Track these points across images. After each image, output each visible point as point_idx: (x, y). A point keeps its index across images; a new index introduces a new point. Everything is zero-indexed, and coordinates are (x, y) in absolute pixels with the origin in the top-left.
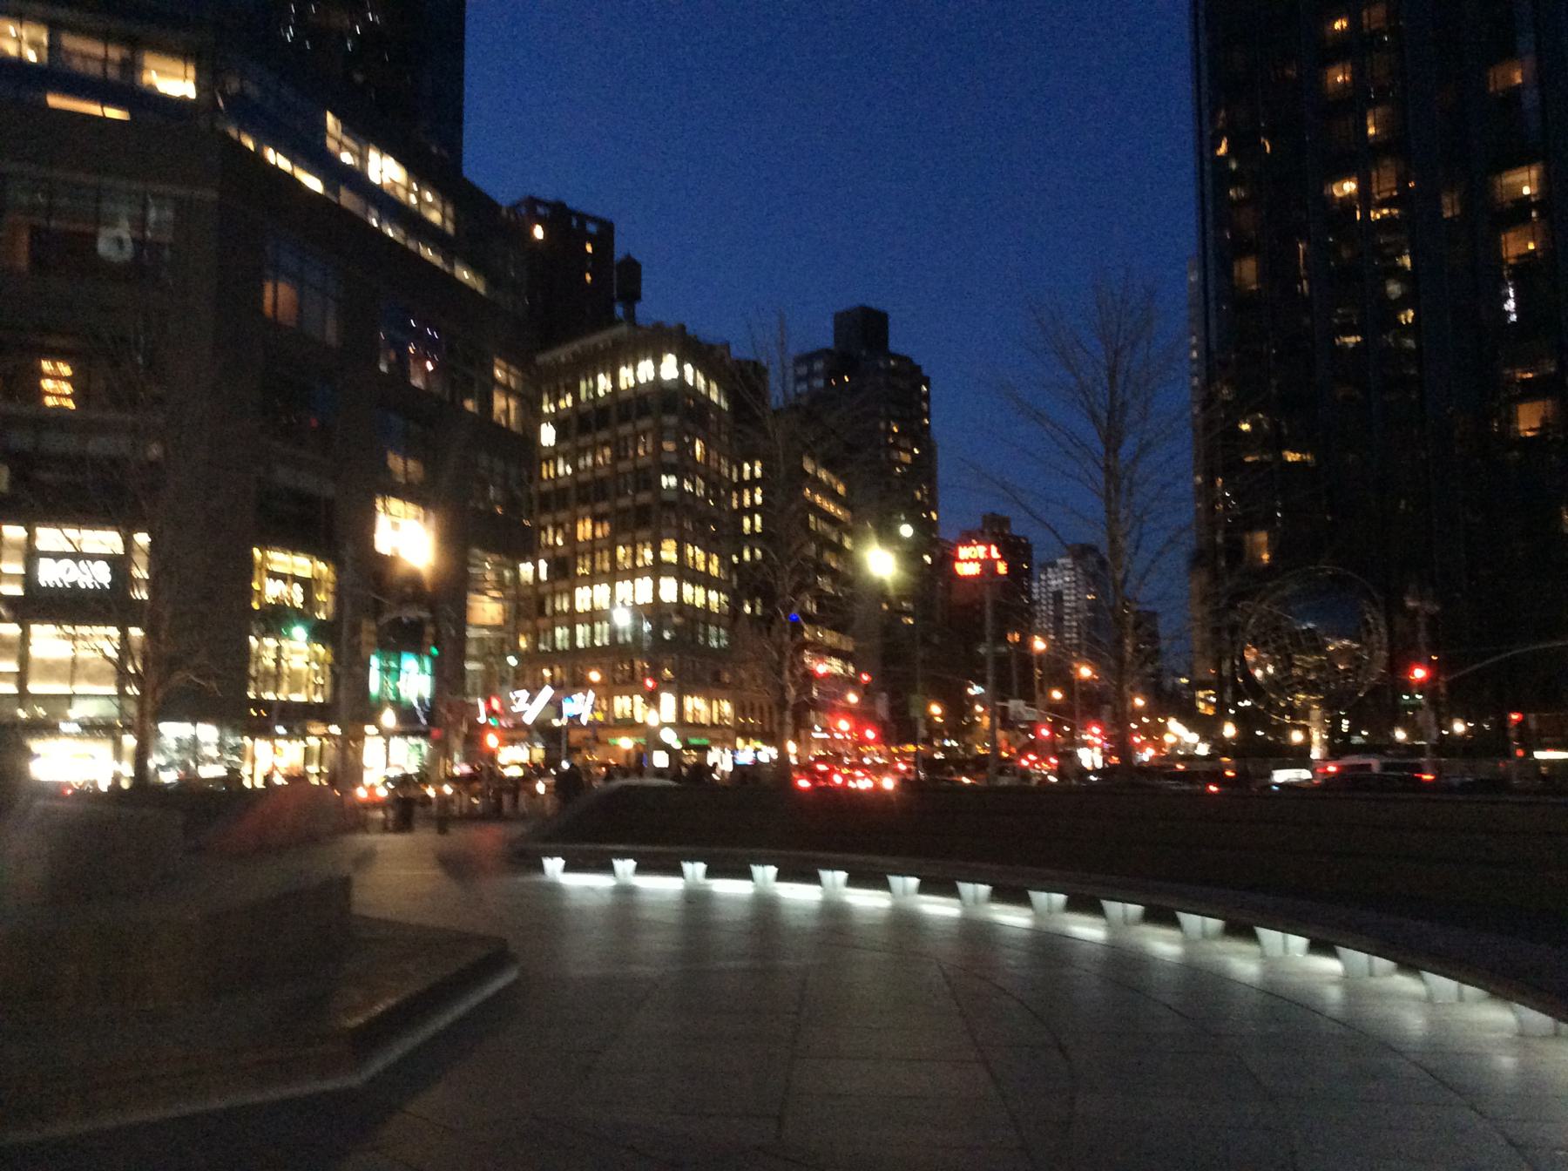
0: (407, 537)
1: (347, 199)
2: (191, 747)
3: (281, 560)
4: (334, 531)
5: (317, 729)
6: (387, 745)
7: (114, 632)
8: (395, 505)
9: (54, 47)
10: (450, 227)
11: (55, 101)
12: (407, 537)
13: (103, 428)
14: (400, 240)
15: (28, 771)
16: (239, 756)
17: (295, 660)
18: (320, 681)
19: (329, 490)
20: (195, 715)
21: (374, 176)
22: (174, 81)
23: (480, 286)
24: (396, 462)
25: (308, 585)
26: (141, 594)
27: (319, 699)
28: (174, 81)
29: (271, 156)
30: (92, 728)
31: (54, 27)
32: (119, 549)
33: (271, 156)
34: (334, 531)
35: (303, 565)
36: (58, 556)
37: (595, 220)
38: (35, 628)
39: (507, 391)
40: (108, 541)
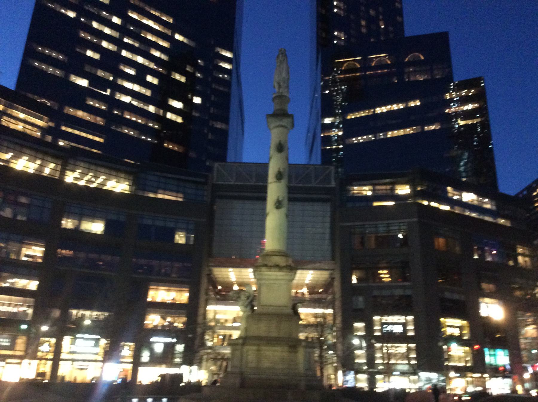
0: (492, 310)
1: (457, 210)
2: (427, 379)
3: (449, 321)
4: (466, 310)
5: (470, 374)
6: (101, 375)
7: (406, 345)
8: (487, 300)
9: (374, 190)
10: (494, 208)
11: (376, 204)
12: (492, 310)
13: (397, 287)
14: (477, 217)
16: (445, 382)
17: (458, 352)
18: (468, 359)
19: (462, 298)
20: (430, 370)
21: (464, 200)
22: (404, 190)
23: (508, 224)
24: (484, 286)
25: (461, 328)
27: (469, 365)
28: (404, 190)
29: (378, 110)
30: (403, 373)
31: (374, 185)
33: (378, 110)
34: (466, 310)
35: (458, 322)
37: (524, 190)
39: (523, 255)
40: (402, 319)
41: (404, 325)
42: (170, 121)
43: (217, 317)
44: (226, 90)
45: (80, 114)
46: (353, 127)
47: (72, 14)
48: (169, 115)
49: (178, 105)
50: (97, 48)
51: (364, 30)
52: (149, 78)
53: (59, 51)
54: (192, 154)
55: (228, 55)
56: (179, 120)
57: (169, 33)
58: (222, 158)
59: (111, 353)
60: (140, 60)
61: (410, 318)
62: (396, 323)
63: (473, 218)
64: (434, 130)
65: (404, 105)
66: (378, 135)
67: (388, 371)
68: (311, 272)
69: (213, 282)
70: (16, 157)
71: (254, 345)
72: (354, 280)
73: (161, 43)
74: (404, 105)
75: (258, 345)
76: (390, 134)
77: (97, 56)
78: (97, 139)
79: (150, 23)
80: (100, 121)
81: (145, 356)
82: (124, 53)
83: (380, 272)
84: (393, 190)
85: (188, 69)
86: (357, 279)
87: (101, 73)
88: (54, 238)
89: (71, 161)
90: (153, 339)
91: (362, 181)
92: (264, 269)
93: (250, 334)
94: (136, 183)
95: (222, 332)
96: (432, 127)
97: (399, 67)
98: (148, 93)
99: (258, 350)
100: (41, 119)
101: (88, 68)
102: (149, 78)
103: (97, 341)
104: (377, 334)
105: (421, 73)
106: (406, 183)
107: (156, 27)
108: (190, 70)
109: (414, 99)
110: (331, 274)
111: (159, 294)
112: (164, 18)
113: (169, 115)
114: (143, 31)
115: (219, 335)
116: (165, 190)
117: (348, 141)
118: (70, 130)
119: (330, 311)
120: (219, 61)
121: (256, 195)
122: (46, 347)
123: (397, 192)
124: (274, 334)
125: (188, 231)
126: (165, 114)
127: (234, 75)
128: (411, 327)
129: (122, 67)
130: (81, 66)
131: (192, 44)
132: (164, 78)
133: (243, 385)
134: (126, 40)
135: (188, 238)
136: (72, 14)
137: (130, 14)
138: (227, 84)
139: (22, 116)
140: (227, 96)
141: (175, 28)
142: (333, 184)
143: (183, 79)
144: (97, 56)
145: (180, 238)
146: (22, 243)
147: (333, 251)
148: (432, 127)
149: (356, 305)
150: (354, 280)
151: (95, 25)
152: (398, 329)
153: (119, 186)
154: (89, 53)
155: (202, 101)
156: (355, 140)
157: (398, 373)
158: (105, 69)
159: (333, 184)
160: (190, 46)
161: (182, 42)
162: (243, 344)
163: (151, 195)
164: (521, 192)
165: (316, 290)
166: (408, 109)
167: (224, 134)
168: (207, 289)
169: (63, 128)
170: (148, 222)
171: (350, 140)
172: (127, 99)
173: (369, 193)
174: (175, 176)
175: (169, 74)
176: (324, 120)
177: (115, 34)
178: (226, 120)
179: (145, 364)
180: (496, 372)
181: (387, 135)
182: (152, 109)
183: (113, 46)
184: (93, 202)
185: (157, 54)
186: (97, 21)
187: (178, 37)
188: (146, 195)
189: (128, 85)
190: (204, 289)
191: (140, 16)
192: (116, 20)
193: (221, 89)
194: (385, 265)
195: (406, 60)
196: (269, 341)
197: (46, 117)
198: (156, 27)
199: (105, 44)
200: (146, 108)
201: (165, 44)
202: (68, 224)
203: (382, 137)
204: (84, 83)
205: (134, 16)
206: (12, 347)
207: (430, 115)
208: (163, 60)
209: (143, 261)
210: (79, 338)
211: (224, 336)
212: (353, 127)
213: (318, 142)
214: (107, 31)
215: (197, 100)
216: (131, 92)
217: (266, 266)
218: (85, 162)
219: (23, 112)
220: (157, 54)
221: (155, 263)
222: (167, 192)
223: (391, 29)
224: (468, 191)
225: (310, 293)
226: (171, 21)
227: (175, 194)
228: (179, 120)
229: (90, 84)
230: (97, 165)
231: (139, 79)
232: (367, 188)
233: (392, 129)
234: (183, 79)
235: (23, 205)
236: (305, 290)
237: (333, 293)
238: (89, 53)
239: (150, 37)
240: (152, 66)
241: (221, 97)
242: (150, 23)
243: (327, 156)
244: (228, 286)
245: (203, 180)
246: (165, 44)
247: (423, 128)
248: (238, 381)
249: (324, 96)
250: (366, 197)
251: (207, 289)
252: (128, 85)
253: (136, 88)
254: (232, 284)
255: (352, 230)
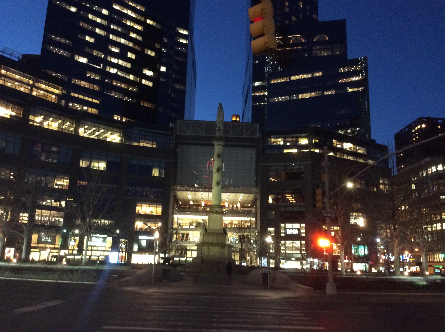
7: (299, 242)
11: (285, 151)
15: (140, 221)
21: (345, 147)
22: (304, 141)
26: (304, 235)
28: (304, 141)
29: (293, 78)
31: (284, 138)
32: (299, 227)
33: (293, 78)
36: (290, 229)
37: (406, 128)
38: (287, 242)
40: (297, 226)
41: (299, 230)
42: (144, 85)
43: (179, 222)
44: (184, 60)
45: (83, 83)
46: (276, 90)
47: (73, 9)
48: (144, 81)
49: (149, 73)
50: (93, 34)
51: (287, 10)
52: (129, 55)
53: (66, 38)
54: (161, 110)
55: (185, 32)
56: (151, 84)
57: (142, 19)
58: (182, 116)
59: (115, 247)
60: (122, 41)
61: (303, 225)
62: (292, 228)
63: (349, 160)
64: (331, 94)
65: (311, 75)
66: (292, 96)
67: (288, 258)
68: (242, 194)
69: (176, 200)
70: (45, 119)
71: (206, 246)
72: (270, 201)
73: (136, 27)
74: (311, 75)
75: (208, 246)
76: (300, 96)
77: (92, 40)
78: (95, 101)
79: (130, 13)
80: (96, 88)
81: (136, 248)
82: (111, 36)
83: (286, 195)
84: (297, 141)
85: (157, 46)
86: (272, 199)
87: (95, 53)
88: (75, 174)
89: (82, 121)
90: (140, 237)
91: (278, 134)
92: (211, 214)
93: (205, 241)
94: (126, 135)
95: (182, 232)
96: (329, 93)
97: (310, 45)
98: (129, 66)
99: (209, 248)
100: (58, 89)
101: (86, 50)
102: (129, 55)
103: (104, 239)
104: (283, 235)
105: (325, 50)
106: (305, 137)
107: (133, 15)
108: (158, 47)
109: (318, 71)
110: (255, 196)
111: (144, 209)
112: (138, 8)
113: (144, 81)
114: (124, 19)
115: (179, 234)
116: (145, 139)
117: (271, 100)
118: (76, 95)
119: (254, 219)
120: (178, 37)
121: (206, 142)
122: (73, 243)
123: (300, 143)
124: (215, 242)
125: (160, 168)
126: (141, 81)
127: (189, 47)
128: (303, 231)
129: (110, 48)
130: (81, 48)
131: (159, 27)
132: (140, 55)
133: (202, 262)
134: (112, 27)
135: (160, 173)
136: (73, 9)
137: (114, 7)
138: (185, 55)
139: (43, 86)
140: (185, 64)
141: (146, 15)
142: (258, 136)
143: (153, 54)
144: (92, 40)
145: (156, 173)
146: (55, 177)
147: (257, 181)
148: (329, 93)
149: (270, 217)
150: (270, 201)
151: (90, 16)
152: (296, 232)
153: (115, 138)
154: (87, 38)
155: (167, 70)
156: (276, 99)
157: (294, 259)
158: (98, 50)
159: (258, 136)
160: (156, 28)
161: (152, 25)
162: (202, 246)
163: (136, 144)
164: (404, 129)
165: (247, 205)
166: (313, 78)
167: (182, 93)
168: (174, 205)
169: (72, 94)
170: (134, 162)
171: (273, 99)
172: (113, 71)
173: (282, 143)
174: (150, 130)
175: (143, 51)
176: (254, 83)
177: (105, 23)
178: (184, 83)
179: (135, 253)
180: (360, 259)
181: (298, 97)
182: (131, 77)
183: (103, 32)
184: (99, 148)
185: (133, 35)
186: (91, 14)
187: (149, 22)
188: (131, 144)
189: (114, 60)
190: (171, 204)
191: (121, 7)
192: (105, 12)
193: (180, 59)
194: (290, 192)
195: (315, 40)
196: (212, 244)
197: (60, 87)
198: (133, 15)
199: (97, 31)
200: (127, 77)
201: (140, 28)
202: (83, 164)
203: (295, 98)
204: (84, 60)
205: (117, 7)
206: (53, 242)
207: (329, 83)
208: (138, 40)
209: (131, 188)
210: (94, 237)
211: (183, 235)
212: (276, 90)
213: (250, 99)
214: (99, 20)
215: (163, 69)
216: (116, 65)
217: (212, 212)
218: (91, 121)
219: (45, 84)
220: (133, 35)
221: (139, 189)
222: (145, 141)
223: (308, 7)
224: (347, 142)
225: (242, 207)
226: (144, 10)
227: (151, 143)
228: (151, 84)
229: (88, 61)
230: (99, 124)
231: (122, 56)
232: (280, 139)
233: (302, 93)
234: (153, 54)
235: (53, 152)
236: (239, 205)
237: (256, 208)
238: (87, 38)
239: (128, 23)
240: (131, 45)
241: (180, 65)
242: (130, 13)
243: (257, 111)
244: (186, 202)
245: (171, 133)
246: (140, 28)
247: (323, 93)
248: (200, 261)
249: (254, 65)
250: (280, 145)
251: (174, 205)
252: (114, 60)
253: (120, 62)
254: (189, 201)
255: (269, 168)
